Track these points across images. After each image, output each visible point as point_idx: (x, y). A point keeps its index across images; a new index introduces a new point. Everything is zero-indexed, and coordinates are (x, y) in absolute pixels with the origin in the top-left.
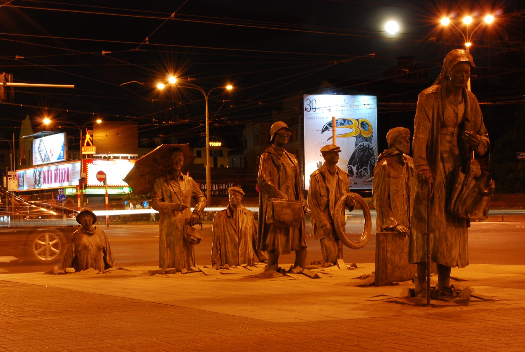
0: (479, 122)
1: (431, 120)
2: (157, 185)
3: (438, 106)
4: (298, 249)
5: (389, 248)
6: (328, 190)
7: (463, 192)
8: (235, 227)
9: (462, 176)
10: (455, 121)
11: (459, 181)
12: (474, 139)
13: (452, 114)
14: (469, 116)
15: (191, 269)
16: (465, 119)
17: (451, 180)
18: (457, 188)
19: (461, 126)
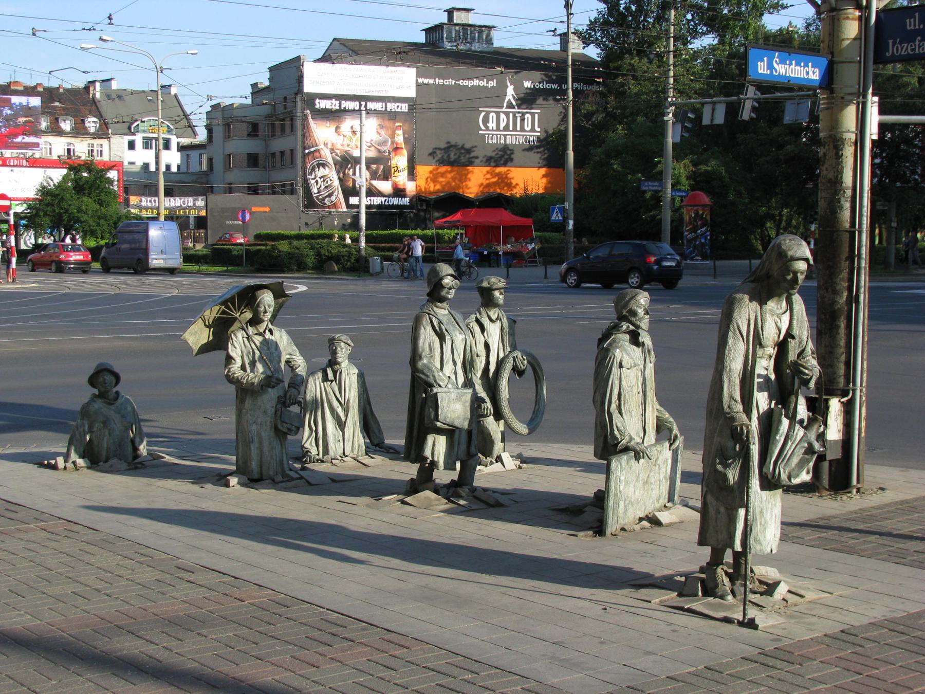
0: (805, 337)
1: (745, 334)
2: (315, 380)
3: (756, 316)
4: (465, 458)
5: (622, 478)
6: (487, 346)
7: (788, 448)
8: (338, 396)
9: (785, 422)
10: (776, 338)
11: (781, 431)
12: (806, 371)
13: (775, 331)
14: (795, 332)
15: (288, 475)
16: (789, 335)
17: (768, 423)
18: (778, 441)
19: (782, 346)
